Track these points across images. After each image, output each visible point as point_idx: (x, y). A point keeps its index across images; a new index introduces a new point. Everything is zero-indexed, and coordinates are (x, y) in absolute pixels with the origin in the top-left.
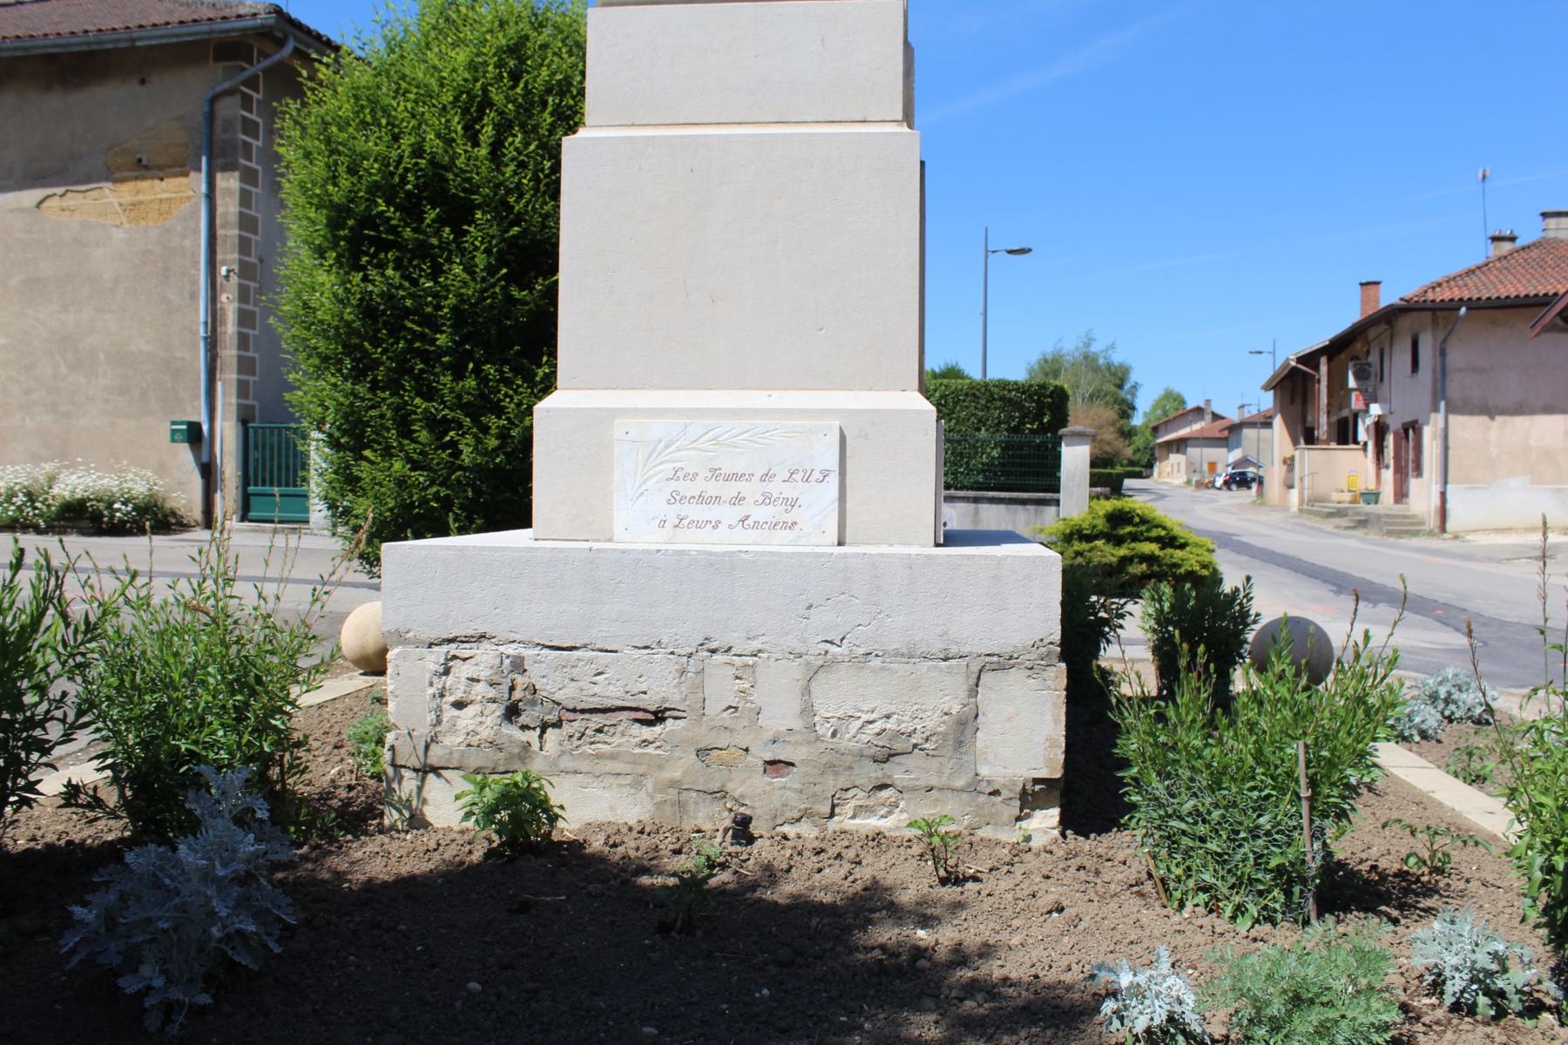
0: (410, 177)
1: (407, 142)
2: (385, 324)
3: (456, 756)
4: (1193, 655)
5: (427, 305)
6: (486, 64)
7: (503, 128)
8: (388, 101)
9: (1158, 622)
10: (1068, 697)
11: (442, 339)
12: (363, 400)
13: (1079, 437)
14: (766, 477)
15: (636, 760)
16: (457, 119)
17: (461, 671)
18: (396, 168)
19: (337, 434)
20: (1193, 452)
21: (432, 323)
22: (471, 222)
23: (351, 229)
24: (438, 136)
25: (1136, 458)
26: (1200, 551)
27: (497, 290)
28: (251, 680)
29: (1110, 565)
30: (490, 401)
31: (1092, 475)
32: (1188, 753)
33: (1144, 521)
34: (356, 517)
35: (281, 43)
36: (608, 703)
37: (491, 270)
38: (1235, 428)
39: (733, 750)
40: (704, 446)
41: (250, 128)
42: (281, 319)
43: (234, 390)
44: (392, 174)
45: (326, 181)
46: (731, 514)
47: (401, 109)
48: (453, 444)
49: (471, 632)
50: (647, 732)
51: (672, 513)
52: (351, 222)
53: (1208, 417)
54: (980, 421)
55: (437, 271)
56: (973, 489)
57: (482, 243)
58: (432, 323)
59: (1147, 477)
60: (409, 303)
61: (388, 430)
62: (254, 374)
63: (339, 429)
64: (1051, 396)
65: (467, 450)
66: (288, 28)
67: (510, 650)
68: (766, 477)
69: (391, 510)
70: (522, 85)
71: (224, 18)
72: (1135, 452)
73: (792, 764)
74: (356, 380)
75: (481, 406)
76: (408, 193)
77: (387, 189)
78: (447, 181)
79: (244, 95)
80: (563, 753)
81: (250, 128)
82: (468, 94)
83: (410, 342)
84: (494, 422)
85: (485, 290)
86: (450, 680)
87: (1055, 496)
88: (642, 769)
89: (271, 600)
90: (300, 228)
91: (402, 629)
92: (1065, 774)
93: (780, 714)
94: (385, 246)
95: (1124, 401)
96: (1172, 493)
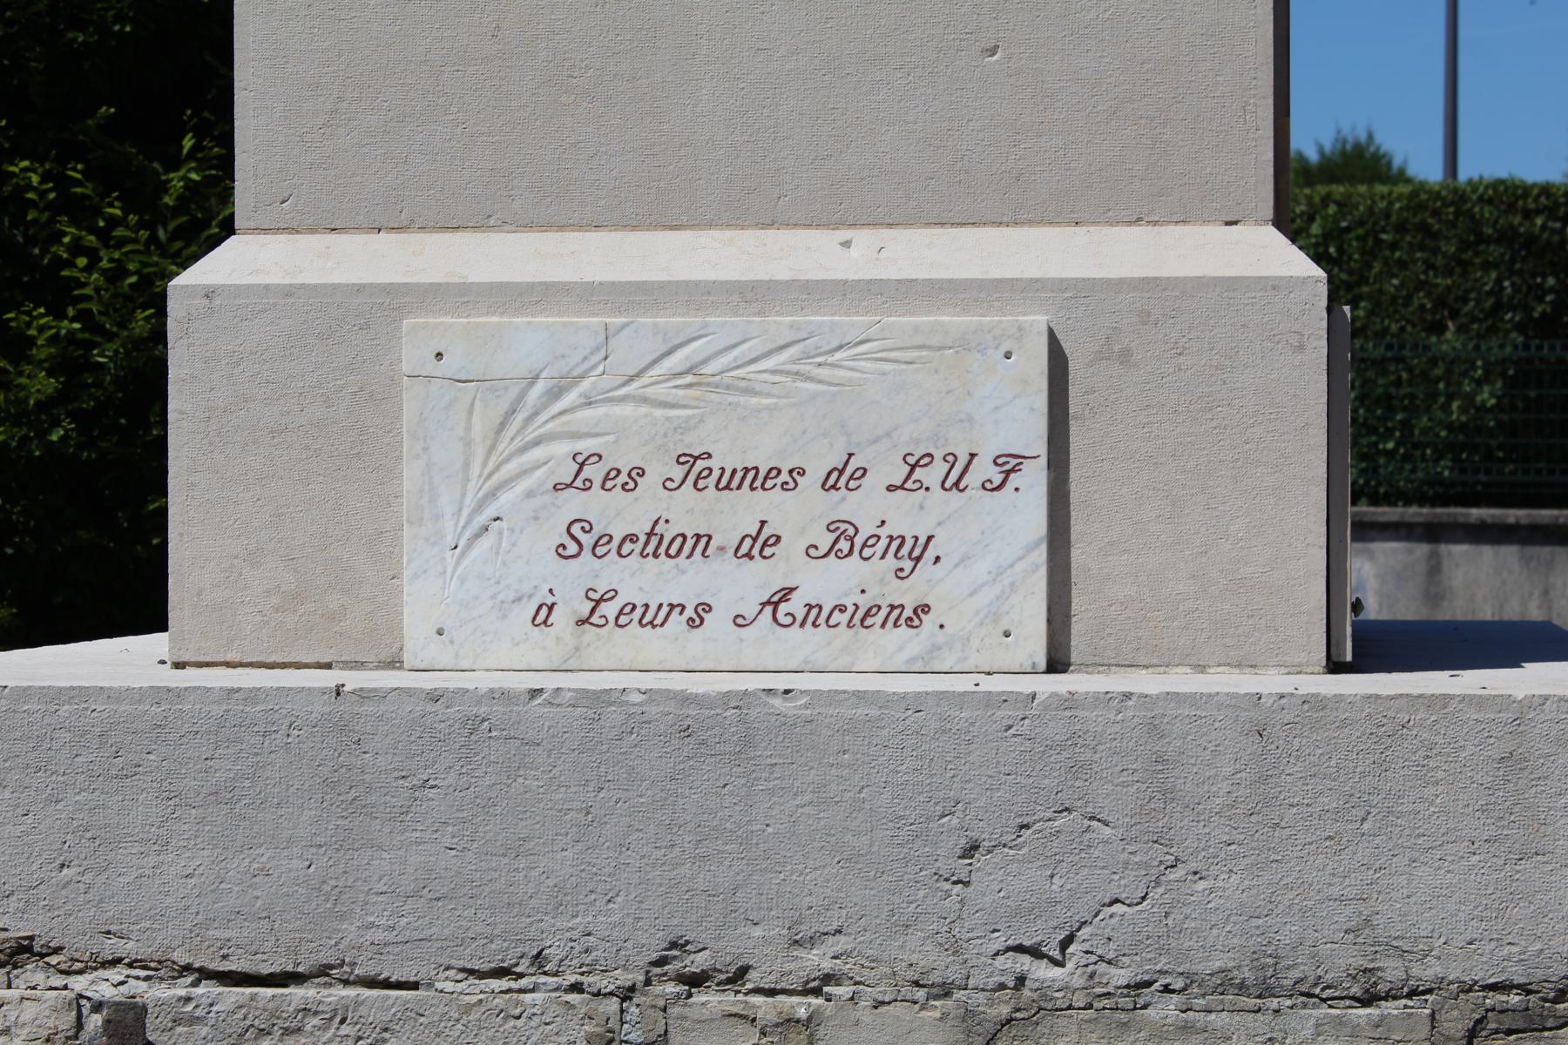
14: (841, 478)
40: (661, 391)
51: (572, 581)
54: (1440, 302)
56: (1422, 500)
67: (104, 986)
68: (841, 478)
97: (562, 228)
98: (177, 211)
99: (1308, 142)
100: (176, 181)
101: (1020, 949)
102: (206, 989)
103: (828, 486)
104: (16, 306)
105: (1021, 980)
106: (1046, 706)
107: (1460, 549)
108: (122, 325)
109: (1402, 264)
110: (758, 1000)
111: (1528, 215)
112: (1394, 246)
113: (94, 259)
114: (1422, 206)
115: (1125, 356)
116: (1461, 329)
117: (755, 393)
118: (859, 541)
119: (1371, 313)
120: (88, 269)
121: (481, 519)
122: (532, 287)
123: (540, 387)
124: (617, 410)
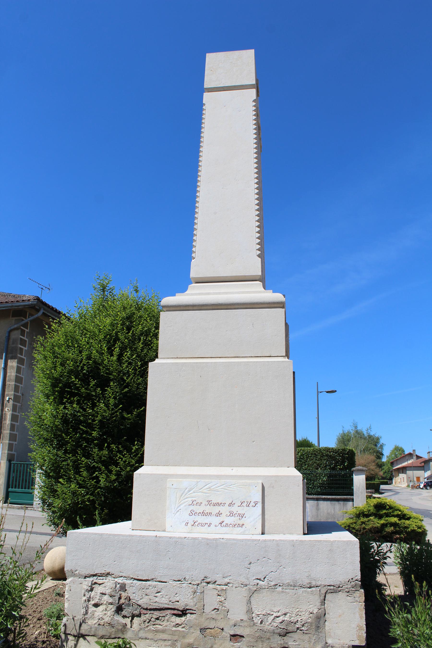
0: (85, 368)
1: (85, 354)
2: (72, 426)
3: (93, 630)
4: (421, 587)
5: (89, 419)
6: (117, 324)
7: (123, 349)
8: (77, 337)
9: (402, 560)
10: (365, 605)
11: (95, 434)
12: (61, 457)
13: (360, 472)
14: (230, 505)
15: (173, 633)
16: (105, 345)
17: (98, 589)
18: (80, 364)
19: (49, 471)
20: (409, 473)
21: (91, 426)
22: (109, 386)
23: (60, 388)
24: (97, 351)
25: (384, 476)
26: (416, 521)
27: (118, 414)
28: (6, 592)
29: (377, 528)
30: (113, 460)
31: (367, 484)
32: (424, 637)
33: (391, 508)
34: (54, 507)
35: (38, 311)
36: (162, 606)
37: (116, 405)
38: (427, 462)
39: (216, 629)
40: (205, 491)
41: (23, 342)
42: (29, 423)
43: (7, 447)
44: (78, 366)
45: (51, 369)
46: (215, 520)
47: (83, 341)
48: (97, 477)
49: (103, 572)
50: (178, 620)
51: (191, 519)
52: (60, 385)
53: (415, 457)
54: (318, 465)
55: (94, 405)
56: (316, 494)
57: (112, 394)
58: (91, 426)
59: (390, 484)
60: (82, 418)
61: (70, 471)
62: (16, 441)
63: (50, 469)
64: (347, 454)
65: (102, 480)
66: (41, 305)
67: (120, 580)
68: (230, 505)
69: (69, 505)
70: (131, 332)
71: (17, 301)
72: (384, 473)
73: (243, 637)
74: (58, 449)
75: (110, 461)
76: (84, 374)
77: (75, 372)
78: (100, 369)
79: (22, 329)
80: (141, 629)
81: (23, 342)
82: (110, 335)
83: (82, 434)
84: (114, 469)
85: (113, 414)
86: (93, 594)
87: (351, 497)
88: (176, 638)
89: (18, 555)
90: (40, 386)
91: (74, 570)
92: (367, 644)
93: (237, 613)
94: (73, 395)
95: (378, 452)
96: (402, 493)
97: (191, 466)
98: (134, 452)
99: (299, 438)
100: (134, 448)
101: (257, 579)
102: (135, 581)
103: (229, 506)
104: (111, 466)
105: (258, 584)
106: (261, 542)
107: (322, 502)
108: (126, 469)
109: (312, 459)
110: (218, 586)
111: (330, 452)
112: (311, 457)
113: (122, 459)
114: (315, 451)
115: (273, 487)
116: (321, 469)
117: (218, 491)
118: (234, 514)
119: (308, 466)
120: (121, 461)
121: (178, 509)
122: (186, 475)
123: (187, 490)
124: (198, 494)
